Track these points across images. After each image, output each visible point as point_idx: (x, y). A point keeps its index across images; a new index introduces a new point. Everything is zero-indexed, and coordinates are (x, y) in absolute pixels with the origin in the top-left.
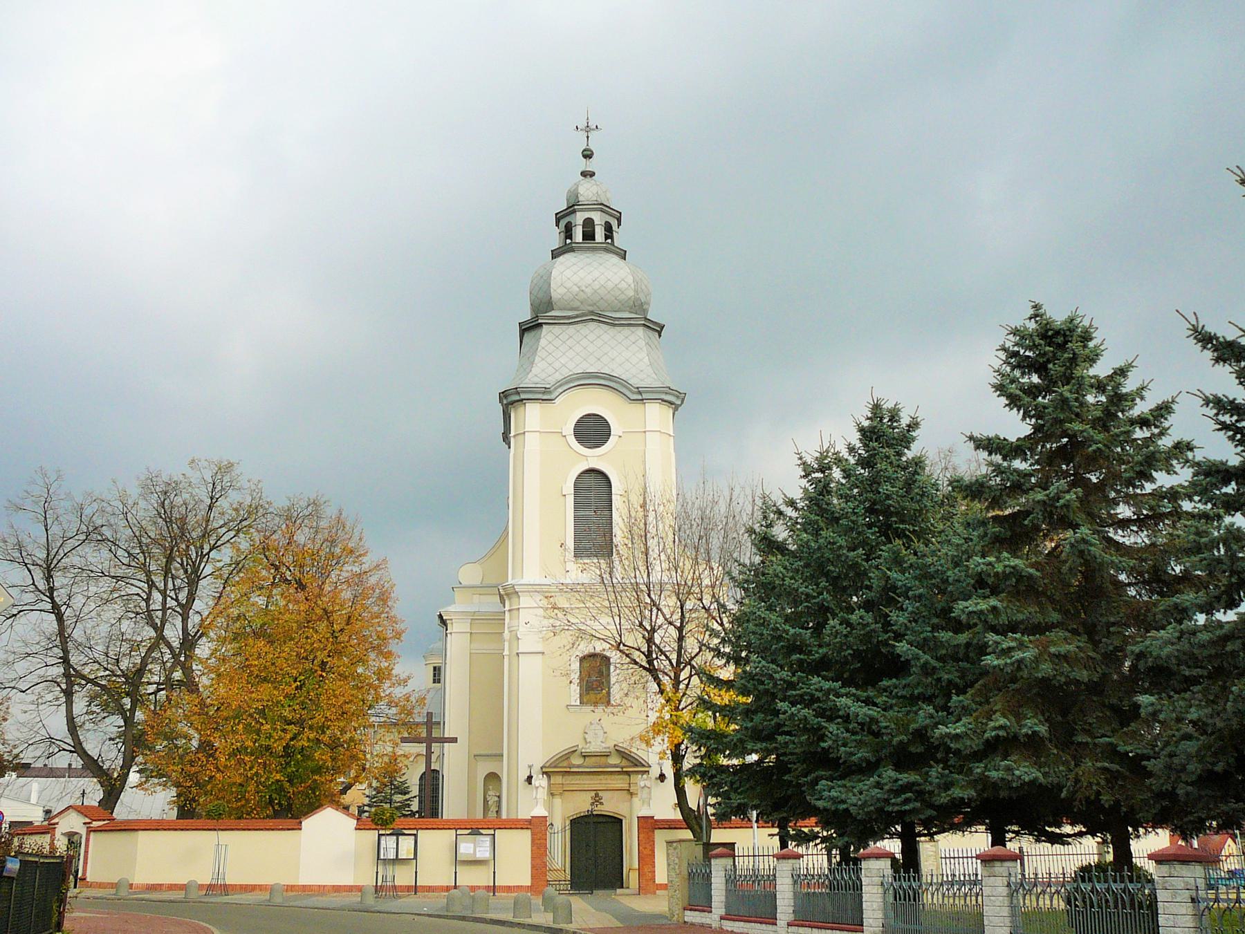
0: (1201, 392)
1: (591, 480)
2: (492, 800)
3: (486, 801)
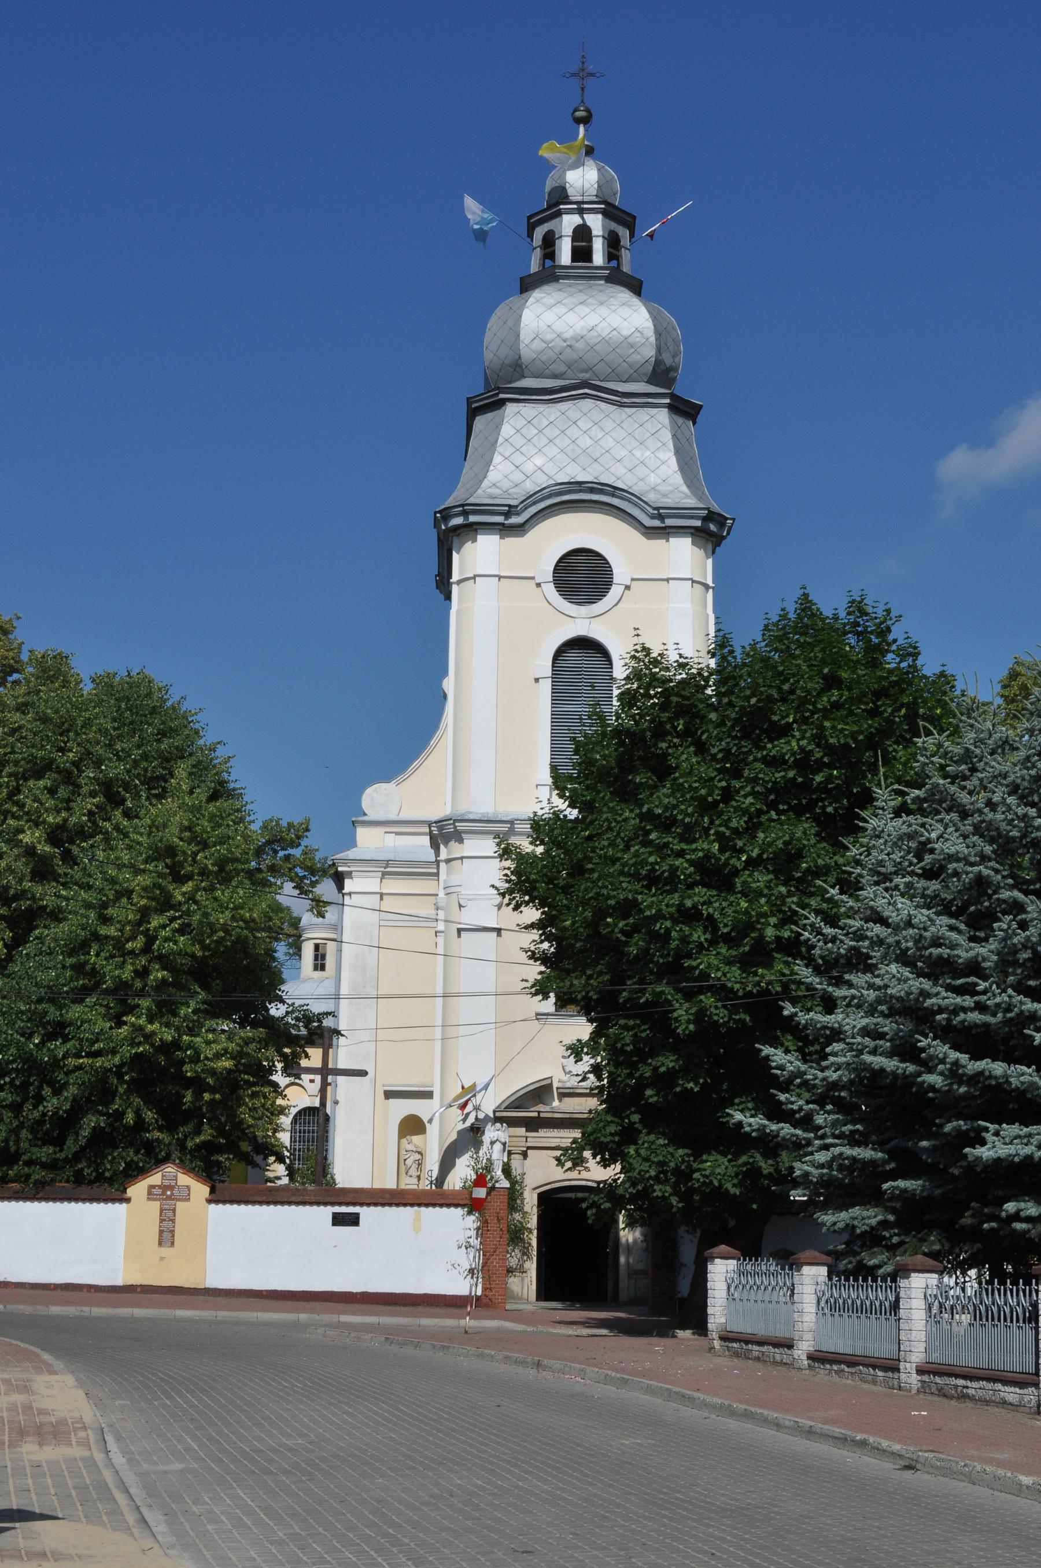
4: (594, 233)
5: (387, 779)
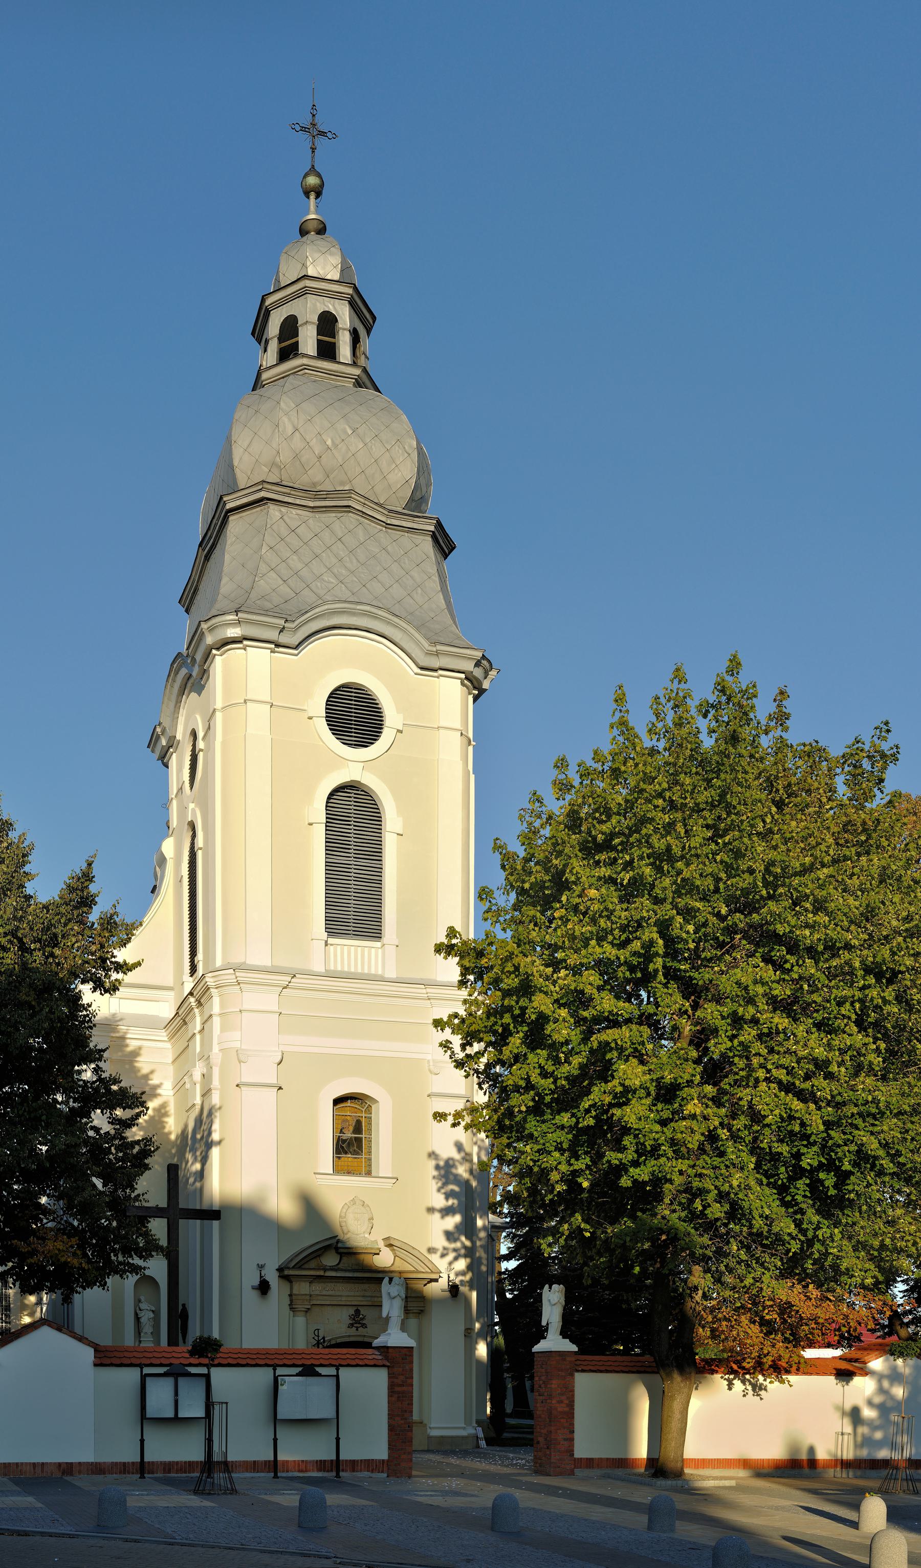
0: (169, 676)
1: (346, 802)
3: (137, 1319)
4: (340, 325)
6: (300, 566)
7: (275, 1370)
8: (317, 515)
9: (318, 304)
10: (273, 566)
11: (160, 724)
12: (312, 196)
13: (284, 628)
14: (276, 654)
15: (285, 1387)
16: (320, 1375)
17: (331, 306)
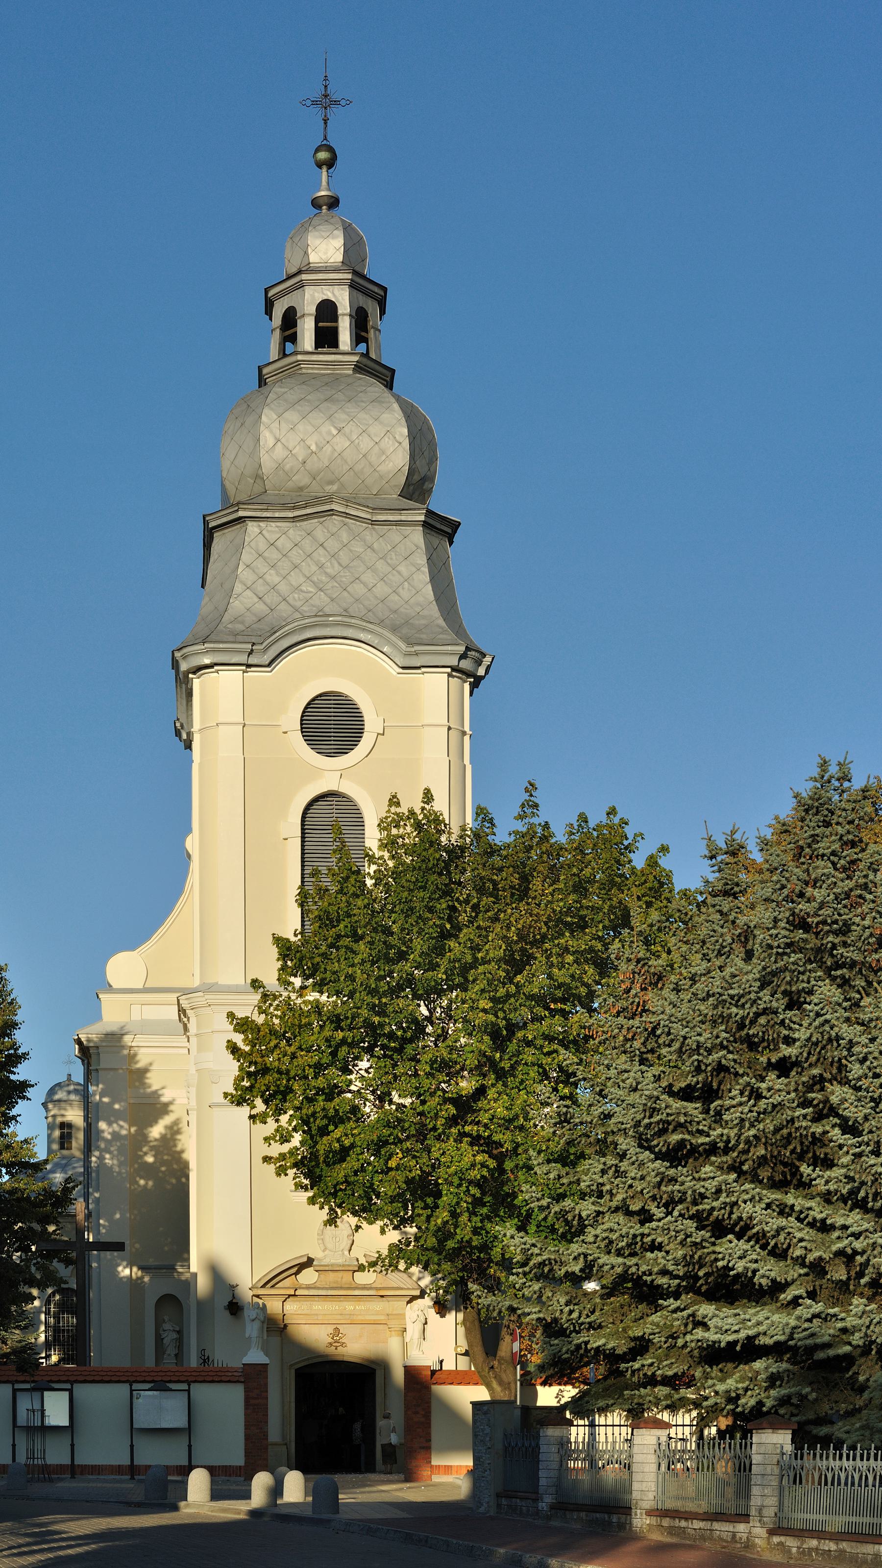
2: (169, 1338)
3: (159, 1339)
4: (340, 311)
5: (132, 947)
6: (276, 579)
7: (131, 1386)
8: (298, 524)
9: (316, 294)
10: (249, 583)
11: (178, 719)
12: (325, 169)
13: (252, 650)
14: (249, 674)
15: (140, 1400)
16: (171, 1390)
17: (327, 293)
